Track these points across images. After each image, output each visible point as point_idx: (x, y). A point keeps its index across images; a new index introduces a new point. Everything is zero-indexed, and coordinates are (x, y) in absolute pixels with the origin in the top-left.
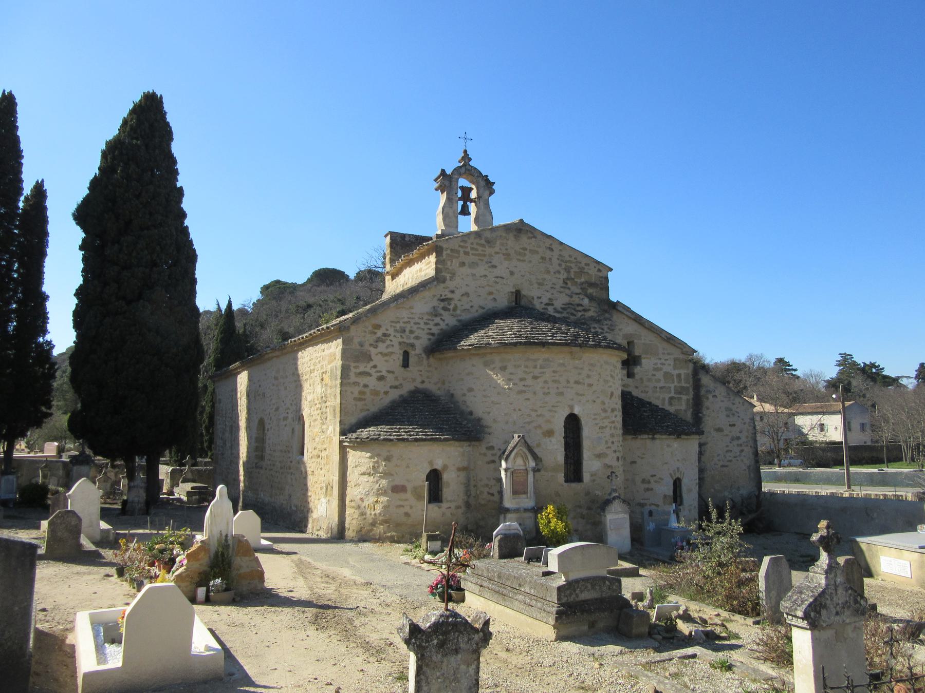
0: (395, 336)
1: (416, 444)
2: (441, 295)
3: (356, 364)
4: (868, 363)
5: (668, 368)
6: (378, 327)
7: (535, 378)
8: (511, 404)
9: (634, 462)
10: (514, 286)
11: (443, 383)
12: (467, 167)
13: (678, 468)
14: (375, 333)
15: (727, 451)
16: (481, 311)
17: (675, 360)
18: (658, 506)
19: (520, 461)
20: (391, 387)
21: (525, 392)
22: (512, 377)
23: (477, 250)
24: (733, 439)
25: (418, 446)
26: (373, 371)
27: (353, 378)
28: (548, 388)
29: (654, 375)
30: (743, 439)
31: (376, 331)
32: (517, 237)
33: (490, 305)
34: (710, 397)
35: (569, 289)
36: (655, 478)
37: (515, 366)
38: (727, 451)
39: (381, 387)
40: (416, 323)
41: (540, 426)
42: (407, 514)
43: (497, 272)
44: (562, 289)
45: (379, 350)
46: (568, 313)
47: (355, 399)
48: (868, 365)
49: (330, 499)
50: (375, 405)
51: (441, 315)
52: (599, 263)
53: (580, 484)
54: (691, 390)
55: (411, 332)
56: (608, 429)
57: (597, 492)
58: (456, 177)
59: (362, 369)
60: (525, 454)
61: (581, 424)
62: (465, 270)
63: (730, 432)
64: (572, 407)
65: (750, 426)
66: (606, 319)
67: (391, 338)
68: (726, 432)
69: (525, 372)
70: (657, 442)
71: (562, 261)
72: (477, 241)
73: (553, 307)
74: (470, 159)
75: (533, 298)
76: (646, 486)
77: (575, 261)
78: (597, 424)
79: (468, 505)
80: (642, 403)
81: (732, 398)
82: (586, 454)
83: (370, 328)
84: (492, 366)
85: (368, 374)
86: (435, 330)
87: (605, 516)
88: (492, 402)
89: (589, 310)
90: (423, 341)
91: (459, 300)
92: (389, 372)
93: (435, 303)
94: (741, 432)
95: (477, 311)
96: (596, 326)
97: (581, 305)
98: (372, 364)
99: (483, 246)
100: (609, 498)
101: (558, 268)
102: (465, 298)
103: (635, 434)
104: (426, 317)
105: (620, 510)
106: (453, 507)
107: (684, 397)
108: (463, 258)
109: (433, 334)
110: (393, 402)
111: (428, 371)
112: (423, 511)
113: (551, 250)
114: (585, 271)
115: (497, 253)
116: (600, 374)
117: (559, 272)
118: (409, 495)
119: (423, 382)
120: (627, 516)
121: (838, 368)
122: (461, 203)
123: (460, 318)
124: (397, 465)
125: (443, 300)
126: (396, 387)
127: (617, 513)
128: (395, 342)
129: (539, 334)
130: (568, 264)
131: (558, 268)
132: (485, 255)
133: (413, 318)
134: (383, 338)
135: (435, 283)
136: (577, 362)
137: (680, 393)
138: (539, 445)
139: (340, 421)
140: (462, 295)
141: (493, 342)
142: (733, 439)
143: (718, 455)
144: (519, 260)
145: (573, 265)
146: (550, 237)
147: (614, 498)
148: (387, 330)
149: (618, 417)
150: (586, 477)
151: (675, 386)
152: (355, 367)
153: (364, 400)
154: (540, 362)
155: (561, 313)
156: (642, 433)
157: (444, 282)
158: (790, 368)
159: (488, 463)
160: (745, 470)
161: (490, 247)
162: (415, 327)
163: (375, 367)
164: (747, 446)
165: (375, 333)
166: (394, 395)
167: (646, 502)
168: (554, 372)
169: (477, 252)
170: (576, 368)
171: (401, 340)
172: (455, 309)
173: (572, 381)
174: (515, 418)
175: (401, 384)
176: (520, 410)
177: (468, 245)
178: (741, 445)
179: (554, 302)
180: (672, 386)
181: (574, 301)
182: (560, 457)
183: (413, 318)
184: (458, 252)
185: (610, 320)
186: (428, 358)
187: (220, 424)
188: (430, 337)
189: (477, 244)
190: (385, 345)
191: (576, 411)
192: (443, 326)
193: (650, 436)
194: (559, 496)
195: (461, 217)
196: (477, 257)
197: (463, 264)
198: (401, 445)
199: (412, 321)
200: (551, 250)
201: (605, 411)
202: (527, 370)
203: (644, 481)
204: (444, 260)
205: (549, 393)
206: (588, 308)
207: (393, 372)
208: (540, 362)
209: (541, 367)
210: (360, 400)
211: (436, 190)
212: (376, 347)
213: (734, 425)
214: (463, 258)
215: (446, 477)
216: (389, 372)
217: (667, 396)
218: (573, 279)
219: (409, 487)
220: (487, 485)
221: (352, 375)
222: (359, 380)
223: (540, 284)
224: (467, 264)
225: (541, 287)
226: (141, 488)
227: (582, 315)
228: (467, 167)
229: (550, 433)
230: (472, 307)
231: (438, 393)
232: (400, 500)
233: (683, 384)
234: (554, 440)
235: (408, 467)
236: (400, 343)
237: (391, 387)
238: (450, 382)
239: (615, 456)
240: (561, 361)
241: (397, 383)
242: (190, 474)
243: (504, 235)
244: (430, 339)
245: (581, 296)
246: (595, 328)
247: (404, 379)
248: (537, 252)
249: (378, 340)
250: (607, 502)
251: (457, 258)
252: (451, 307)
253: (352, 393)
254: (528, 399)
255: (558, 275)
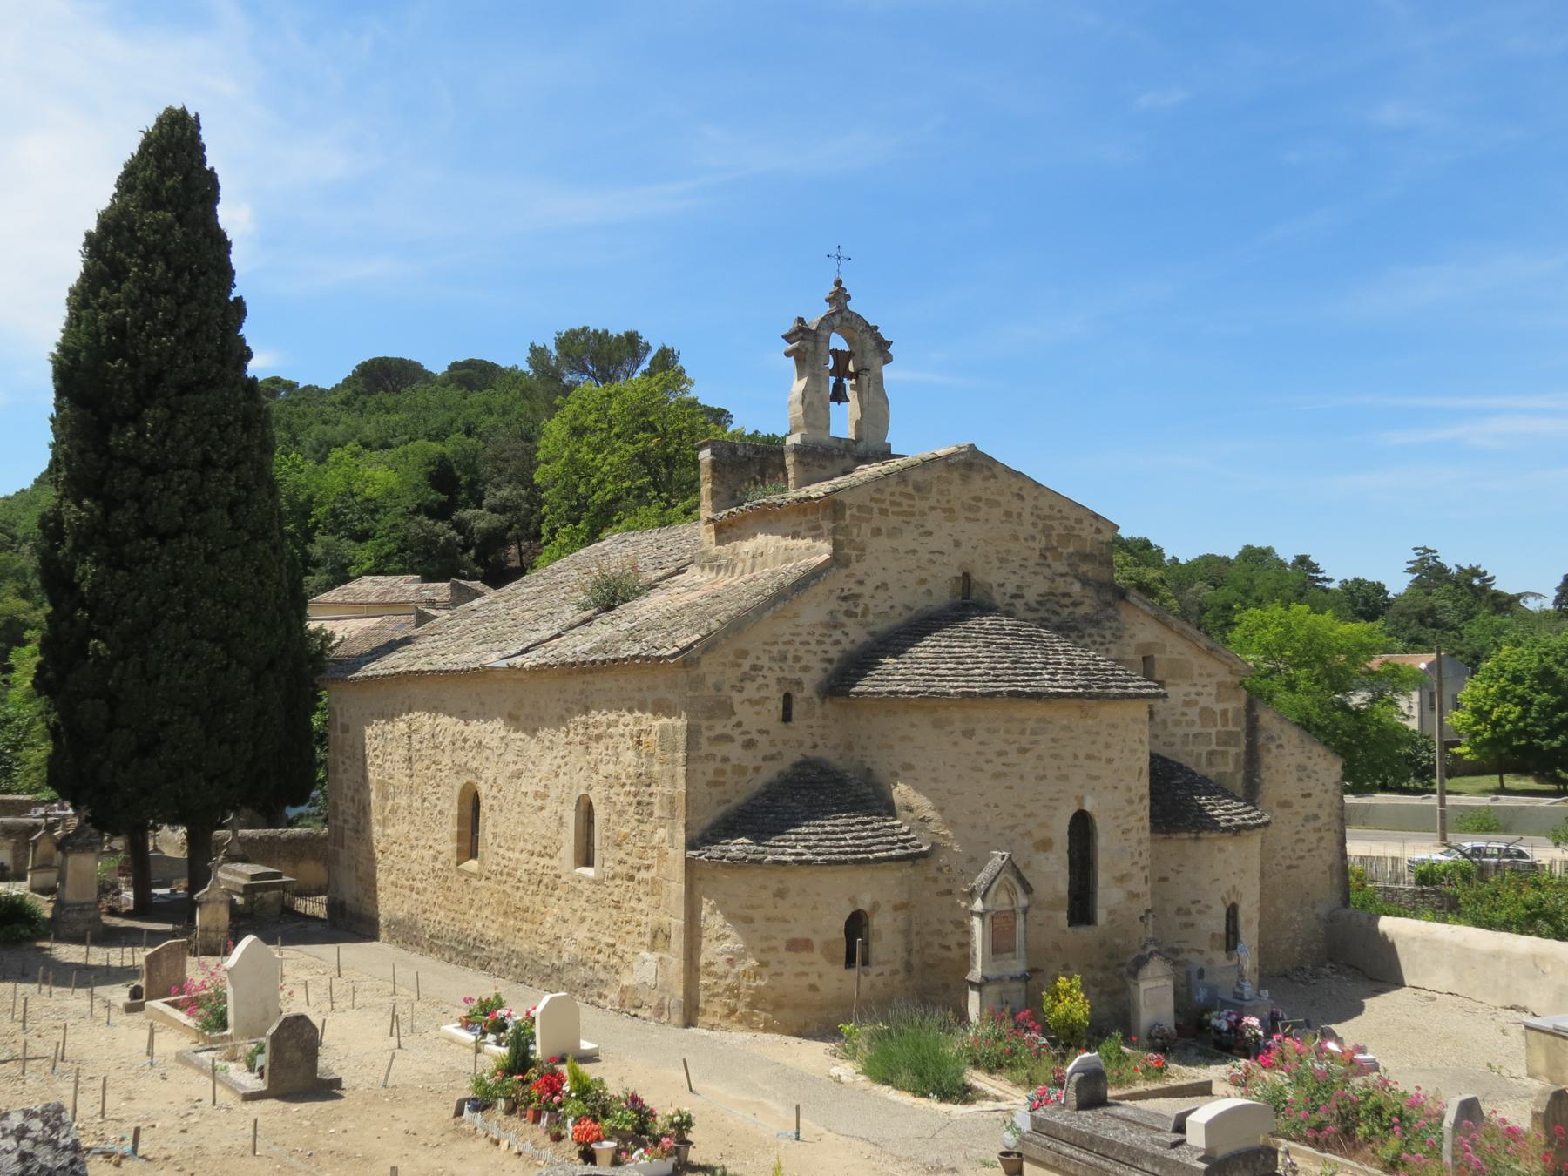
0: (770, 669)
1: (830, 868)
2: (843, 590)
3: (710, 722)
4: (1466, 567)
5: (1204, 701)
6: (743, 654)
7: (1023, 751)
8: (982, 795)
9: (1165, 879)
10: (960, 567)
11: (850, 747)
12: (845, 314)
13: (1234, 887)
14: (739, 666)
15: (1298, 841)
16: (907, 615)
17: (1219, 685)
18: (1201, 952)
19: (1003, 898)
20: (765, 759)
21: (1005, 774)
22: (982, 749)
23: (900, 504)
24: (1307, 819)
25: (833, 872)
26: (736, 733)
27: (705, 748)
28: (1044, 768)
29: (1184, 714)
30: (1324, 819)
31: (740, 661)
32: (965, 479)
33: (922, 603)
34: (1273, 746)
35: (1049, 566)
36: (1198, 906)
37: (988, 730)
38: (1298, 841)
39: (750, 759)
40: (802, 644)
41: (1029, 834)
42: (813, 988)
43: (934, 543)
44: (1038, 569)
45: (745, 695)
46: (1047, 610)
47: (709, 784)
48: (1465, 571)
49: (665, 956)
50: (741, 790)
51: (843, 625)
52: (1096, 517)
53: (1091, 927)
54: (1243, 736)
55: (797, 659)
56: (1134, 831)
57: (1118, 941)
58: (826, 333)
59: (719, 730)
60: (1012, 884)
61: (1094, 827)
62: (883, 542)
63: (1304, 807)
64: (1081, 800)
65: (1334, 794)
66: (1109, 618)
67: (765, 672)
68: (1296, 808)
69: (1006, 741)
70: (1204, 845)
71: (1038, 516)
72: (901, 488)
73: (1023, 601)
74: (848, 298)
75: (991, 587)
76: (1185, 919)
77: (1059, 515)
78: (1118, 826)
79: (908, 967)
80: (1165, 760)
81: (1308, 748)
82: (1103, 877)
83: (731, 657)
84: (949, 729)
85: (728, 739)
86: (834, 653)
87: (1137, 985)
88: (949, 791)
89: (1081, 603)
90: (814, 675)
91: (872, 597)
92: (761, 732)
93: (834, 604)
94: (1320, 806)
95: (900, 615)
96: (1093, 631)
97: (1069, 595)
98: (734, 720)
99: (910, 497)
100: (1142, 953)
101: (1031, 531)
102: (881, 594)
103: (1167, 832)
104: (819, 631)
105: (1159, 973)
106: (887, 973)
107: (1233, 751)
108: (877, 520)
109: (830, 661)
110: (769, 785)
111: (824, 727)
112: (835, 979)
113: (1021, 498)
114: (1075, 533)
115: (933, 508)
116: (1124, 741)
117: (1033, 538)
118: (816, 955)
119: (815, 746)
120: (1170, 983)
121: (1411, 577)
122: (833, 380)
123: (872, 628)
124: (795, 905)
125: (845, 599)
126: (772, 758)
127: (1156, 978)
128: (772, 681)
129: (1027, 675)
130: (1048, 522)
131: (1031, 531)
132: (912, 514)
133: (798, 635)
134: (753, 673)
135: (834, 569)
136: (1090, 722)
137: (1226, 744)
138: (1027, 865)
139: (686, 825)
140: (877, 588)
141: (952, 691)
142: (1307, 819)
143: (1283, 849)
144: (968, 519)
145: (1055, 523)
146: (1018, 475)
147: (1151, 954)
148: (758, 658)
149: (1143, 810)
150: (1102, 916)
151: (1218, 732)
152: (710, 728)
153: (723, 783)
154: (1030, 725)
155: (1036, 610)
156: (1179, 830)
157: (847, 566)
158: (1320, 576)
159: (941, 894)
160: (1324, 872)
161: (922, 499)
162: (802, 649)
163: (739, 724)
164: (1329, 830)
165: (739, 666)
166: (770, 773)
167: (1182, 945)
168: (1053, 740)
169: (901, 509)
170: (1088, 733)
171: (781, 675)
172: (865, 613)
173: (1081, 755)
174: (988, 819)
175: (780, 753)
176: (996, 806)
177: (886, 496)
178: (1320, 830)
179: (1025, 592)
180: (1213, 731)
181: (1056, 588)
182: (1063, 887)
183: (798, 635)
184: (870, 510)
185: (1116, 620)
186: (823, 702)
187: (346, 771)
188: (826, 665)
189: (902, 494)
190: (755, 685)
191: (1087, 808)
192: (846, 644)
193: (1193, 835)
194: (1060, 949)
195: (833, 405)
196: (901, 518)
197: (877, 532)
198: (804, 870)
199: (798, 640)
200: (1021, 498)
201: (1130, 802)
202: (1009, 737)
203: (1179, 911)
204: (847, 526)
205: (1045, 777)
206: (1080, 599)
207: (767, 732)
208: (1030, 725)
209: (1033, 733)
210: (715, 784)
211: (787, 354)
212: (741, 690)
213: (1309, 795)
214: (877, 520)
215: (876, 923)
216: (761, 732)
217: (1204, 750)
218: (1055, 549)
219: (817, 941)
220: (939, 932)
221: (704, 741)
222: (714, 750)
223: (1002, 560)
224: (884, 530)
225: (1004, 565)
226: (221, 902)
227: (1070, 614)
228: (845, 314)
229: (1045, 845)
230: (892, 607)
231: (840, 765)
232: (803, 964)
233: (1231, 728)
234: (1052, 856)
235: (815, 908)
236: (779, 680)
237: (765, 759)
238: (864, 748)
239: (1142, 875)
240: (1065, 722)
241: (774, 751)
242: (238, 846)
243: (944, 475)
244: (825, 670)
245: (1069, 579)
246: (1090, 635)
247: (785, 743)
248: (998, 504)
249: (744, 678)
250: (1141, 962)
251: (868, 521)
252: (859, 610)
253: (704, 773)
254: (1011, 788)
255: (1031, 543)
